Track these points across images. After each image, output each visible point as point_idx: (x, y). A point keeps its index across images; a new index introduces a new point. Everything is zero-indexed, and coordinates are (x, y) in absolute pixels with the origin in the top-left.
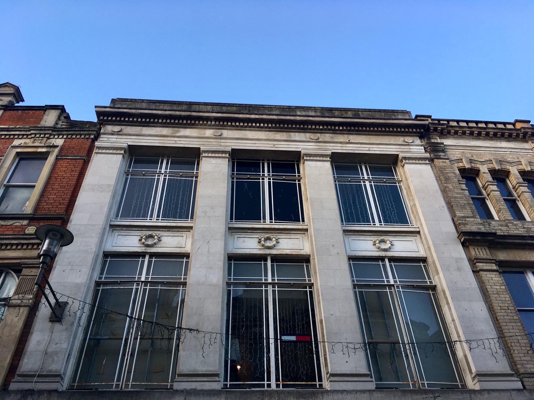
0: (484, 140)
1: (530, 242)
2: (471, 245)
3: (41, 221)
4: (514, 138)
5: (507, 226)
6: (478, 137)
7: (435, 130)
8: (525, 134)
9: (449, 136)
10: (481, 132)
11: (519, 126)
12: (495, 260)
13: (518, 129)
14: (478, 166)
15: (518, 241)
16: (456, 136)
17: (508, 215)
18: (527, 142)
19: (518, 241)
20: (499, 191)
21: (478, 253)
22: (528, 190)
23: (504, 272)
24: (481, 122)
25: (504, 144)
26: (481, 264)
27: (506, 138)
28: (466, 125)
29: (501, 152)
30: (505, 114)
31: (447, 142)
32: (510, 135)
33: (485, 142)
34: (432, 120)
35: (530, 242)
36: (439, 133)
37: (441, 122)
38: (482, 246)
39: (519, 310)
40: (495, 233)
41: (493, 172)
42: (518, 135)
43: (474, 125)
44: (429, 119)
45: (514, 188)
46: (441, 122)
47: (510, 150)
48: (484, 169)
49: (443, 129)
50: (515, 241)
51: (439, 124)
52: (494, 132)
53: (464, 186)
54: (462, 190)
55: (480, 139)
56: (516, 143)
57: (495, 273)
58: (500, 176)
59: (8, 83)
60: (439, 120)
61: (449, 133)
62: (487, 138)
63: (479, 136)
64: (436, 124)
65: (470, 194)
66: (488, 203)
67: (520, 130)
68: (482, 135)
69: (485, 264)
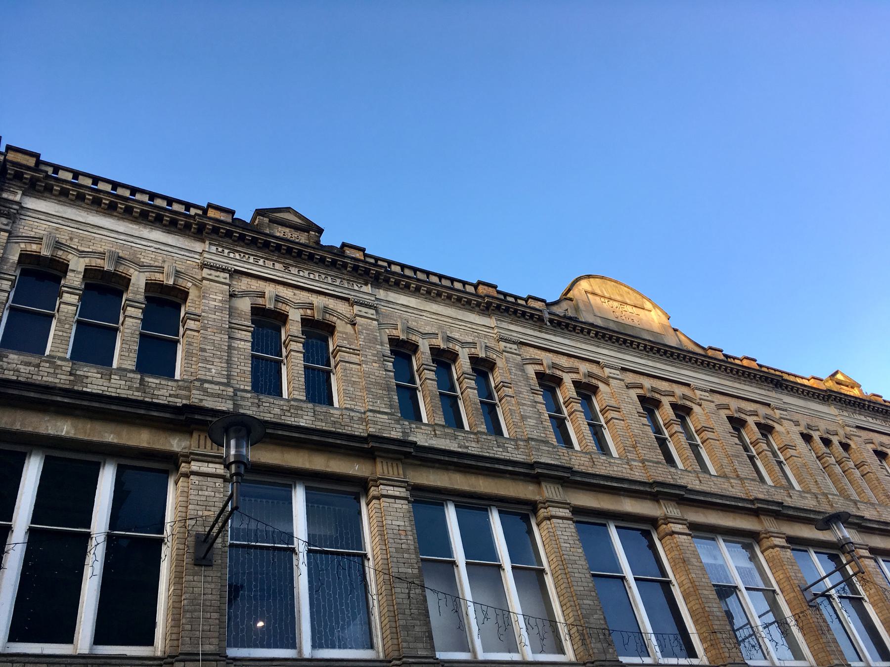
0: (120, 218)
1: (59, 399)
2: (545, 481)
3: (37, 382)
4: (180, 229)
5: (189, 389)
6: (109, 212)
7: (18, 176)
8: (489, 304)
9: (49, 195)
10: (116, 203)
11: (482, 290)
12: (407, 482)
13: (480, 297)
14: (457, 348)
15: (32, 395)
16: (417, 294)
17: (592, 446)
18: (489, 316)
19: (32, 395)
20: (142, 320)
21: (386, 472)
22: (581, 409)
23: (415, 502)
24: (143, 192)
25: (157, 235)
26: (554, 509)
27: (165, 225)
28: (183, 211)
29: (139, 245)
30: (466, 269)
31: (31, 203)
32: (407, 286)
33: (121, 222)
34: (366, 255)
35: (59, 399)
36: (25, 183)
37: (380, 263)
38: (558, 483)
39: (594, 575)
40: (686, 487)
41: (436, 352)
42: (418, 289)
43: (108, 188)
44: (361, 253)
45: (751, 443)
46: (380, 263)
47: (158, 246)
48: (424, 346)
49: (378, 274)
50: (497, 466)
51: (376, 265)
52: (142, 210)
53: (540, 398)
54: (386, 370)
55: (111, 215)
56: (181, 239)
57: (402, 502)
58: (443, 359)
59: (288, 210)
60: (377, 259)
61: (387, 281)
62: (127, 216)
63: (111, 210)
64: (370, 264)
65: (306, 359)
66: (420, 395)
67: (483, 298)
68: (119, 210)
69: (391, 488)
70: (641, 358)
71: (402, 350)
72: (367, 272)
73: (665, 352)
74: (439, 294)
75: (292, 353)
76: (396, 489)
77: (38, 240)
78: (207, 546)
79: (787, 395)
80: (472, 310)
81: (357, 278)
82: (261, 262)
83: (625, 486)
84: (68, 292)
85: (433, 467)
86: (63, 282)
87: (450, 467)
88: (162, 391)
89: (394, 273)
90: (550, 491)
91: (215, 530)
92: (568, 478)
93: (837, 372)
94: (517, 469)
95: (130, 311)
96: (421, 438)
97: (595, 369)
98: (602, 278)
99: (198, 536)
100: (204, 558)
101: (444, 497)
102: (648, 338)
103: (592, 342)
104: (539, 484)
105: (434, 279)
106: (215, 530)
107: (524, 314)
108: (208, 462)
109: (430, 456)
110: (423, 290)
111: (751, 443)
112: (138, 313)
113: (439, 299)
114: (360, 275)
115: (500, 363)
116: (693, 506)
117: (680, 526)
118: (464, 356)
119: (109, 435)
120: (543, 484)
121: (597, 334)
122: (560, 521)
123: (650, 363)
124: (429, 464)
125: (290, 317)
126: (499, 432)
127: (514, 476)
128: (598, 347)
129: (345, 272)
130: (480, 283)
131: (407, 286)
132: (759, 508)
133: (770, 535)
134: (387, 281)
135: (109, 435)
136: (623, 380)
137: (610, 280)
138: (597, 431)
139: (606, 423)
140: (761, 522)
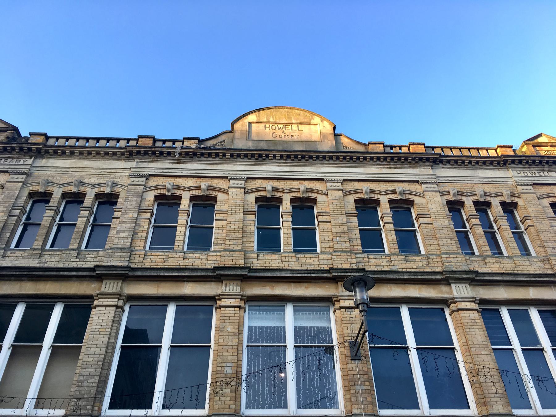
41: (503, 204)
44: (423, 147)
61: (47, 152)
70: (278, 166)
71: (454, 207)
72: (30, 149)
73: (484, 163)
74: (90, 153)
75: (474, 226)
76: (109, 300)
77: (104, 184)
78: (356, 349)
79: (450, 168)
80: (119, 159)
81: (24, 155)
82: (22, 162)
83: (187, 274)
84: (473, 218)
85: (10, 280)
86: (216, 209)
87: (23, 278)
88: (415, 264)
89: (51, 146)
90: (458, 290)
91: (359, 338)
92: (474, 279)
93: (540, 135)
94: (80, 273)
95: (285, 218)
96: (477, 266)
97: (214, 183)
98: (275, 108)
99: (350, 343)
100: (356, 355)
101: (16, 300)
102: (301, 148)
103: (229, 162)
104: (449, 284)
105: (102, 143)
106: (359, 338)
107: (161, 153)
108: (108, 298)
109: (5, 273)
110: (77, 152)
111: (494, 221)
112: (289, 218)
113: (91, 156)
114: (25, 153)
115: (520, 202)
116: (40, 280)
117: (233, 300)
118: (495, 202)
119: (533, 293)
120: (453, 286)
121: (232, 156)
122: (104, 308)
123: (159, 165)
124: (7, 278)
125: (415, 202)
126: (528, 254)
127: (80, 278)
128: (235, 165)
129: (14, 153)
130: (139, 137)
131: (64, 153)
132: (333, 276)
133: (340, 298)
134: (47, 152)
135: (533, 293)
136: (535, 193)
137: (283, 108)
138: (519, 237)
139: (498, 230)
140: (337, 288)
